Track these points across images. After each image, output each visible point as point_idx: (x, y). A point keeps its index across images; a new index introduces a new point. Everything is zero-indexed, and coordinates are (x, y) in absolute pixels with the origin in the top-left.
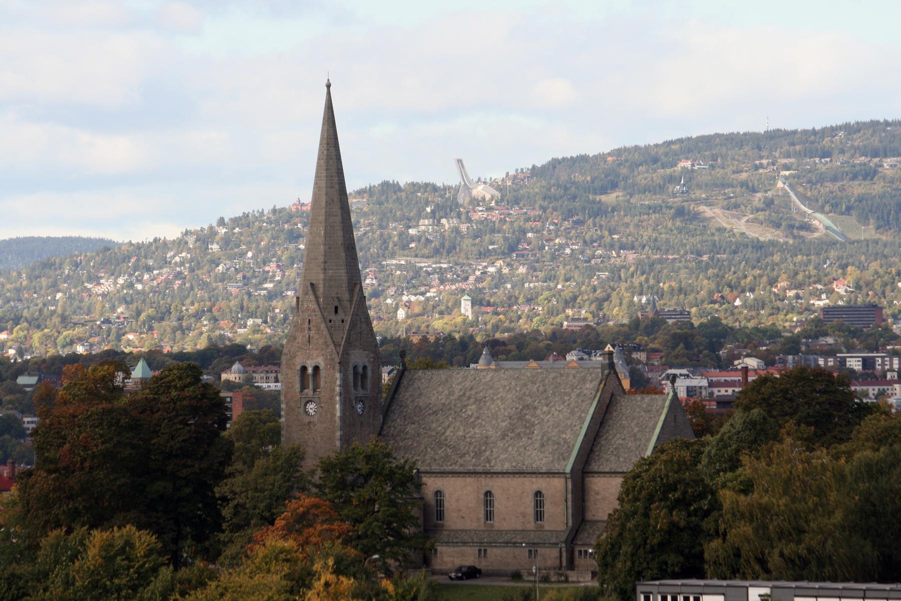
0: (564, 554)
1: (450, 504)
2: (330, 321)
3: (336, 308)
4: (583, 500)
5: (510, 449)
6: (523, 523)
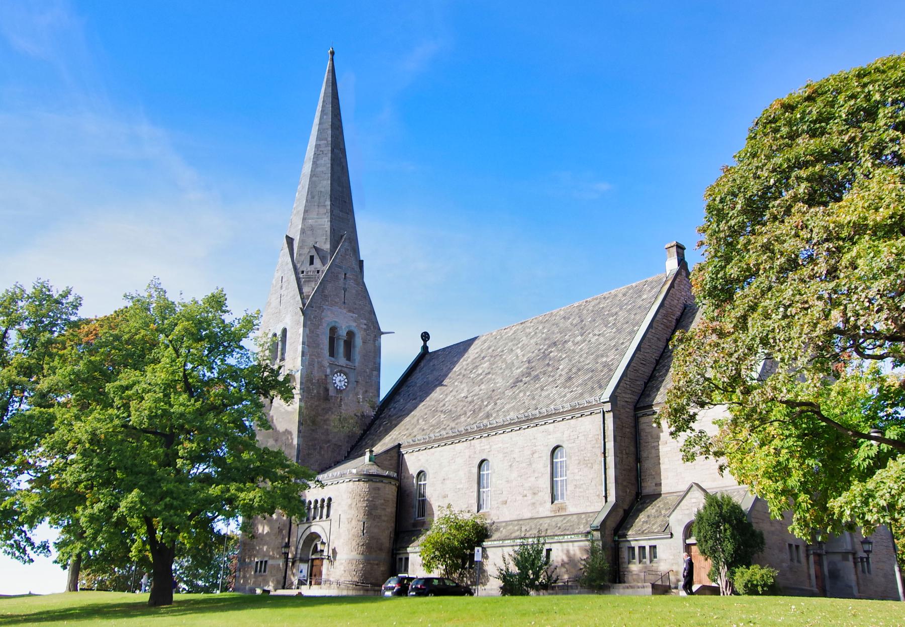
3: (312, 258)
4: (638, 459)
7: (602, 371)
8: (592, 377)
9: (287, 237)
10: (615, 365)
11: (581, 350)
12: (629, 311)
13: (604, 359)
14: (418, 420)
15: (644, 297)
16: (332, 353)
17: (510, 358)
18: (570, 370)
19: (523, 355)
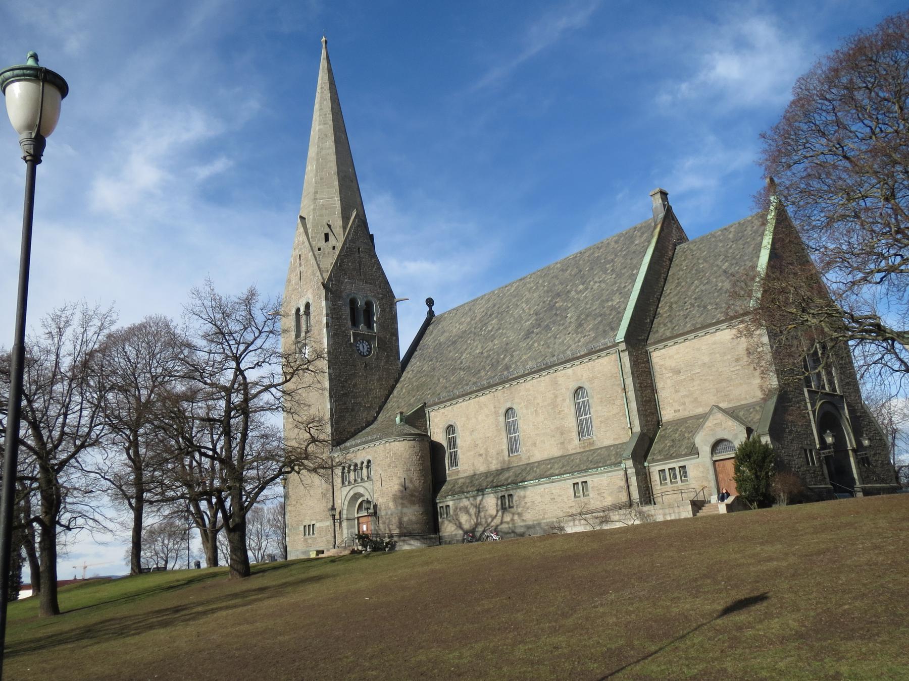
0: (633, 480)
2: (319, 249)
3: (327, 236)
5: (536, 345)
6: (562, 443)
7: (610, 314)
8: (602, 321)
9: (301, 217)
10: (622, 307)
11: (586, 297)
12: (625, 257)
13: (610, 304)
14: (439, 379)
15: (637, 242)
16: (355, 324)
17: (517, 312)
18: (579, 317)
19: (529, 309)
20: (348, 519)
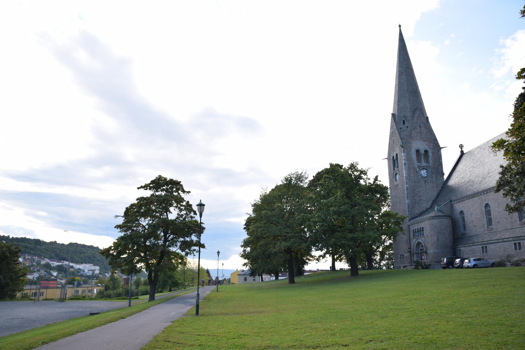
1: (468, 218)
3: (404, 121)
4: (453, 228)
20: (416, 253)
